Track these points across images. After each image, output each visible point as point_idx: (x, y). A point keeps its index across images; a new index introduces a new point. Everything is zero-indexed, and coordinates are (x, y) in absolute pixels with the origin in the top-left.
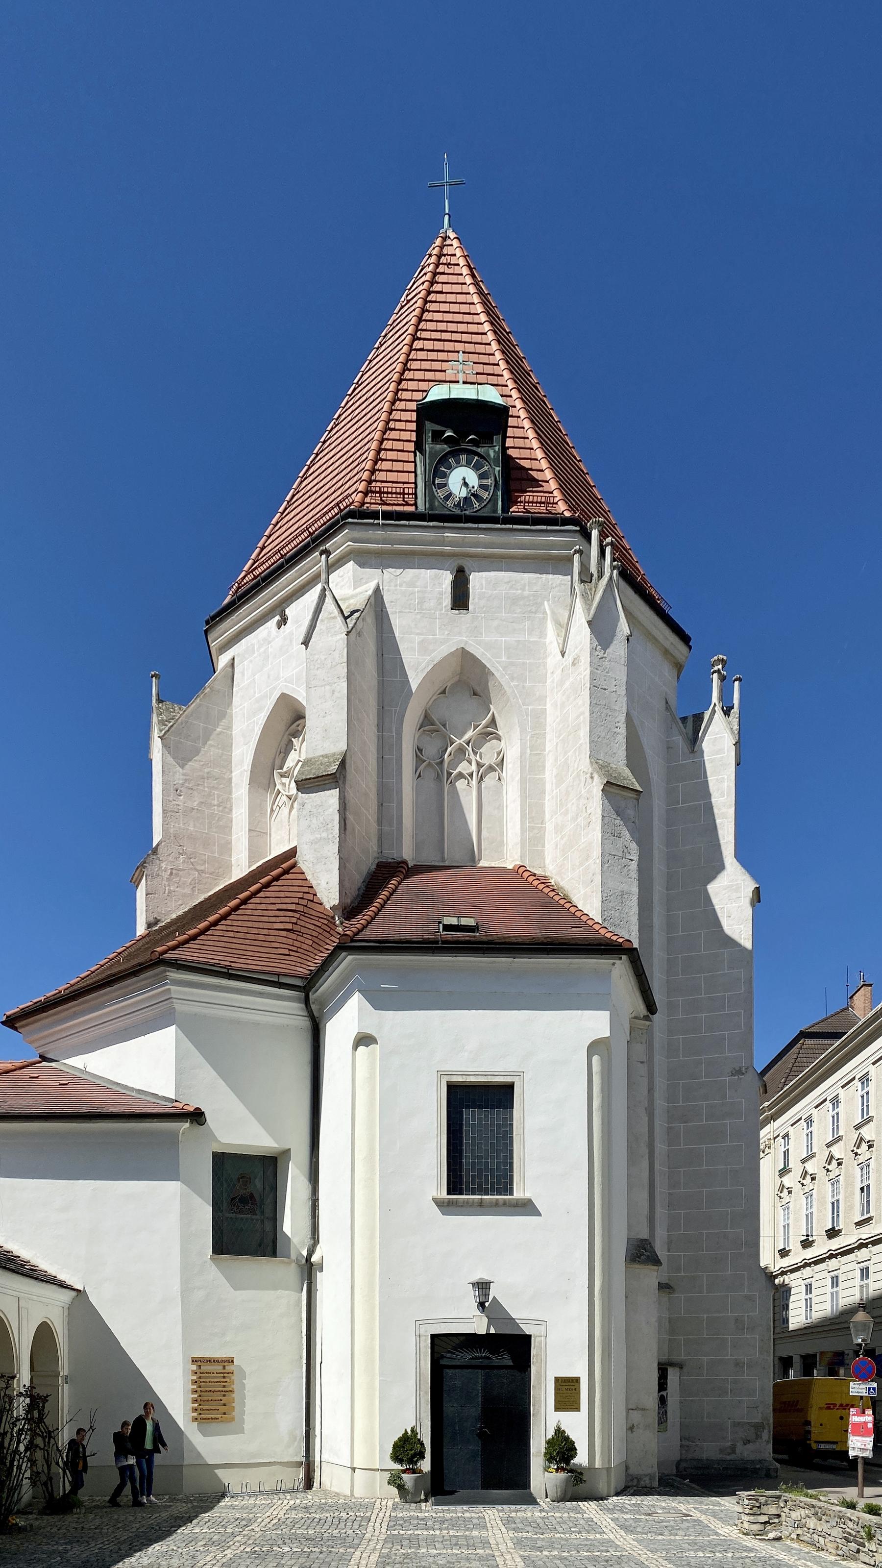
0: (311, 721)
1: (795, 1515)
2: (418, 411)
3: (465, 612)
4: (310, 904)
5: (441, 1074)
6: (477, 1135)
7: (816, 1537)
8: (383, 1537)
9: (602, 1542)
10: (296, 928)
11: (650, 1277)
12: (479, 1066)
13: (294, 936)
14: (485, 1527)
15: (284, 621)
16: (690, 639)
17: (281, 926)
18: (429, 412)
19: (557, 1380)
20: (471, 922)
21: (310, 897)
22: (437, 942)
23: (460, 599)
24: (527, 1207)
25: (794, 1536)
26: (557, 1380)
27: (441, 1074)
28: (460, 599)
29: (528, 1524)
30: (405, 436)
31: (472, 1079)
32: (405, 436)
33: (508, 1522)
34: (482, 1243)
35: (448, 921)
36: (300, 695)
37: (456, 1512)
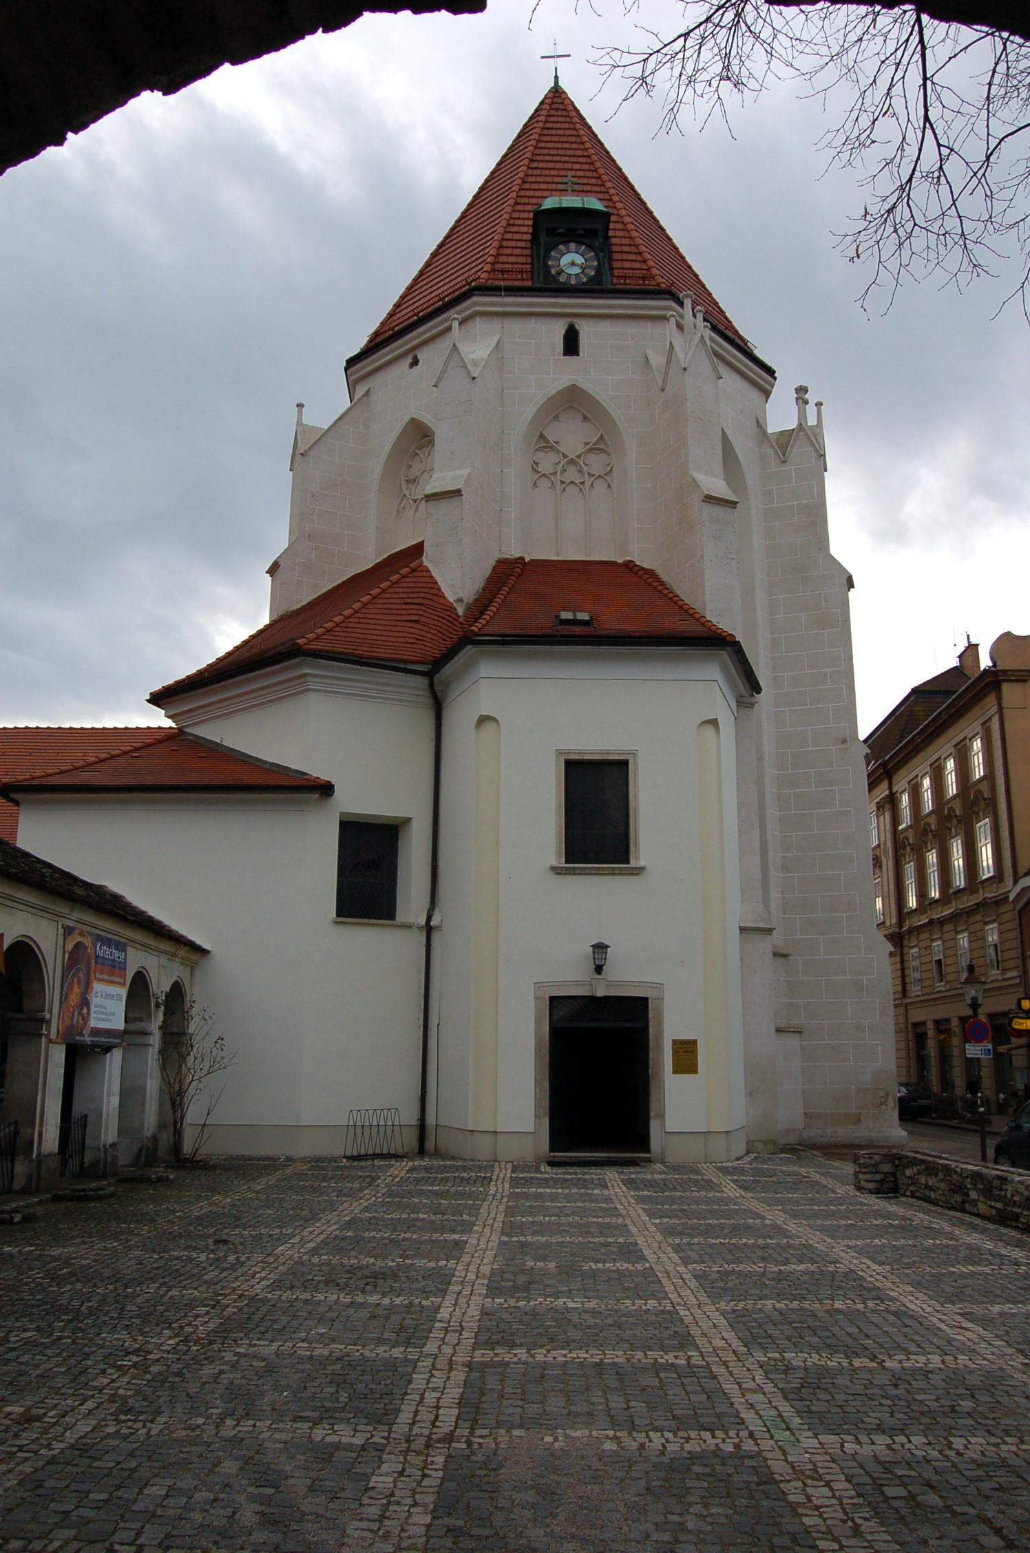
0: (439, 438)
1: (908, 1172)
2: (534, 219)
3: (572, 757)
4: (435, 598)
5: (559, 753)
6: (597, 815)
7: (927, 1192)
8: (506, 1193)
9: (722, 1199)
10: (422, 619)
11: (764, 946)
12: (595, 743)
13: (421, 627)
14: (606, 1186)
15: (415, 362)
16: (774, 372)
17: (408, 618)
18: (541, 216)
19: (674, 1042)
20: (583, 616)
21: (436, 592)
22: (555, 636)
23: (571, 345)
24: (638, 871)
25: (908, 1193)
26: (674, 1042)
27: (559, 753)
28: (571, 345)
29: (649, 1185)
30: (526, 222)
31: (611, 757)
32: (525, 229)
33: (629, 1183)
34: (598, 900)
35: (566, 615)
36: (428, 419)
37: (576, 1174)
